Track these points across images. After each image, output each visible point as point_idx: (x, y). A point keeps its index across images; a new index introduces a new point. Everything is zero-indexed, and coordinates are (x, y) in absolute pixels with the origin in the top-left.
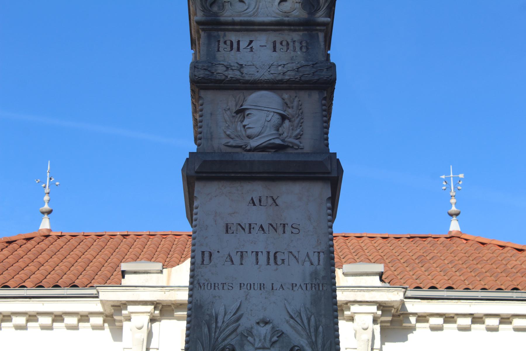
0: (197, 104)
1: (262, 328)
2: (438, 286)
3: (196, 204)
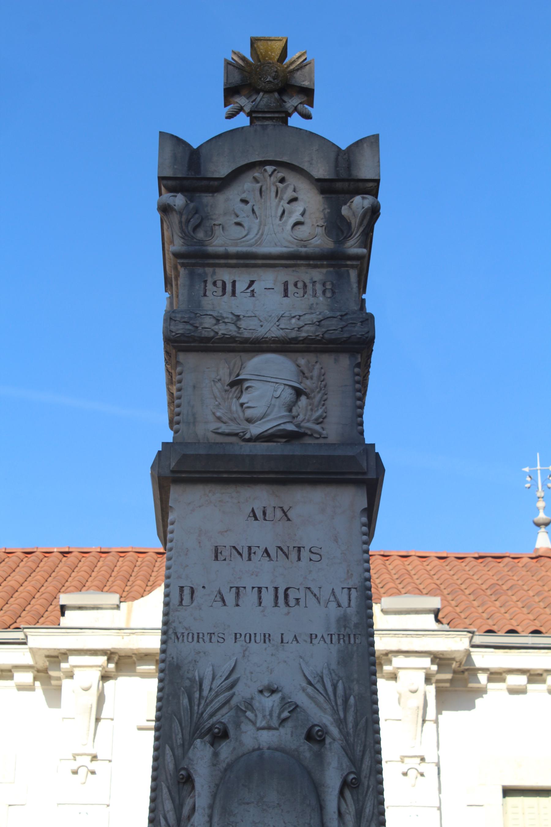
0: (173, 372)
1: (267, 699)
2: (519, 629)
3: (171, 517)
